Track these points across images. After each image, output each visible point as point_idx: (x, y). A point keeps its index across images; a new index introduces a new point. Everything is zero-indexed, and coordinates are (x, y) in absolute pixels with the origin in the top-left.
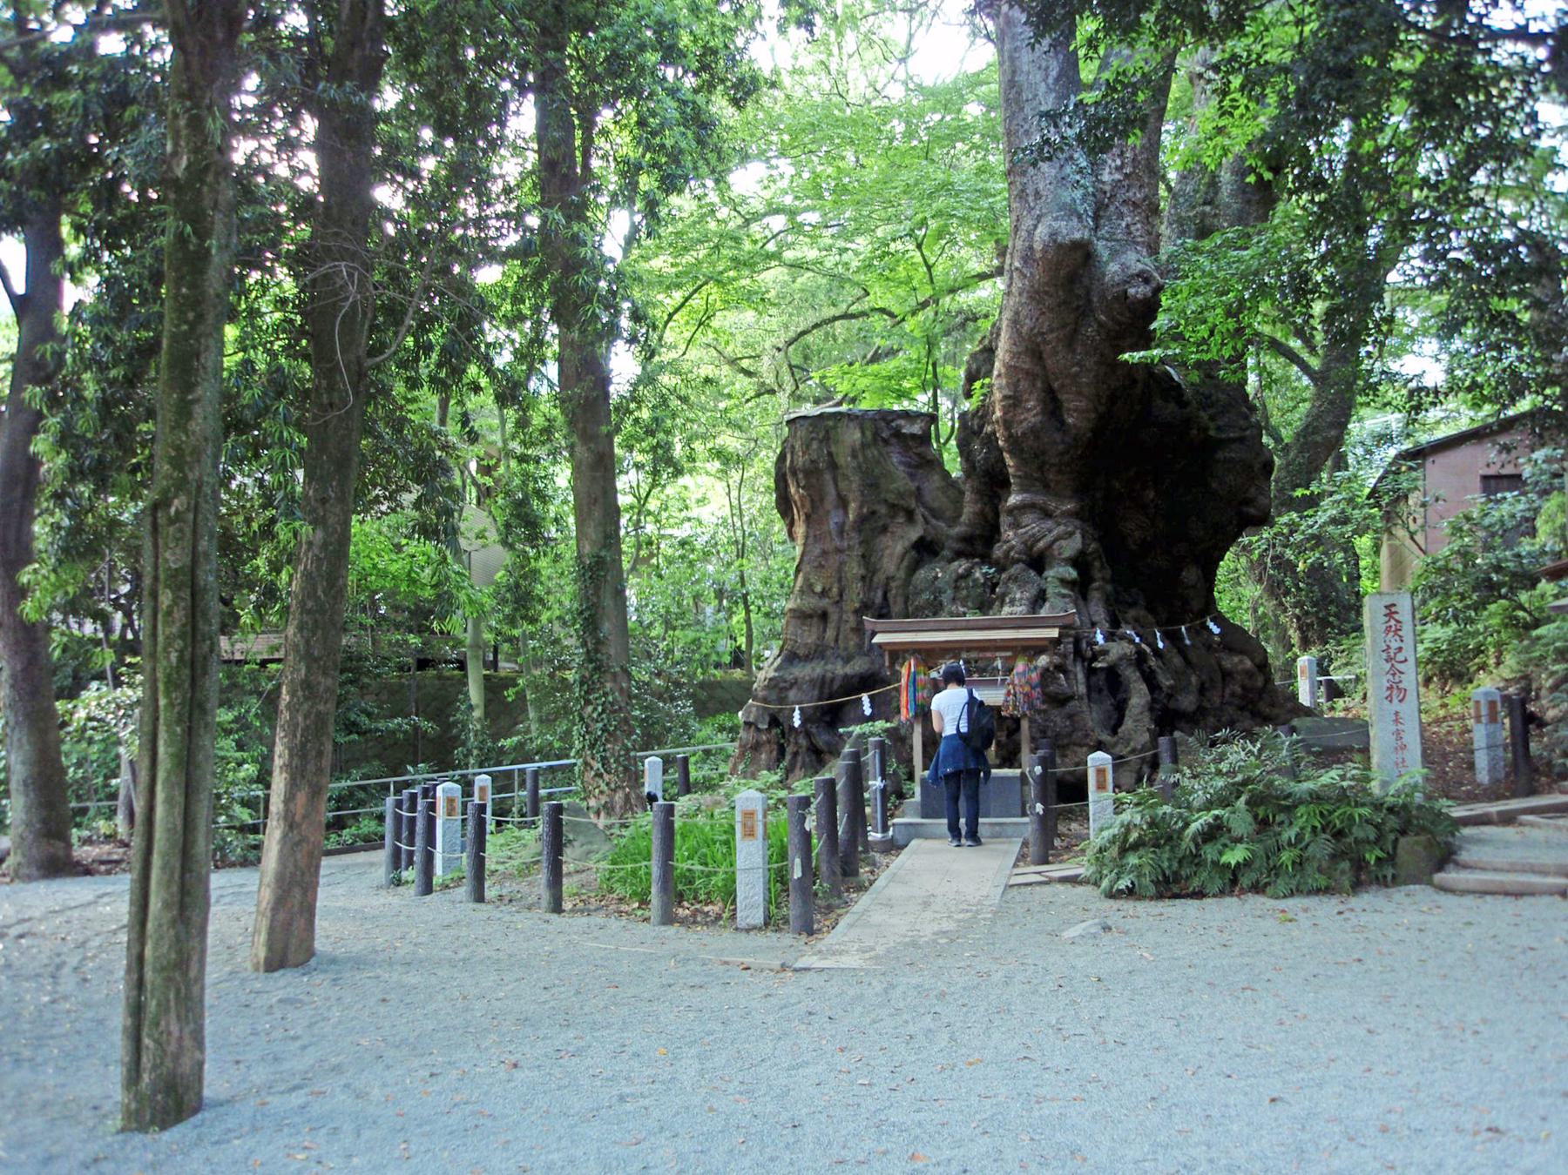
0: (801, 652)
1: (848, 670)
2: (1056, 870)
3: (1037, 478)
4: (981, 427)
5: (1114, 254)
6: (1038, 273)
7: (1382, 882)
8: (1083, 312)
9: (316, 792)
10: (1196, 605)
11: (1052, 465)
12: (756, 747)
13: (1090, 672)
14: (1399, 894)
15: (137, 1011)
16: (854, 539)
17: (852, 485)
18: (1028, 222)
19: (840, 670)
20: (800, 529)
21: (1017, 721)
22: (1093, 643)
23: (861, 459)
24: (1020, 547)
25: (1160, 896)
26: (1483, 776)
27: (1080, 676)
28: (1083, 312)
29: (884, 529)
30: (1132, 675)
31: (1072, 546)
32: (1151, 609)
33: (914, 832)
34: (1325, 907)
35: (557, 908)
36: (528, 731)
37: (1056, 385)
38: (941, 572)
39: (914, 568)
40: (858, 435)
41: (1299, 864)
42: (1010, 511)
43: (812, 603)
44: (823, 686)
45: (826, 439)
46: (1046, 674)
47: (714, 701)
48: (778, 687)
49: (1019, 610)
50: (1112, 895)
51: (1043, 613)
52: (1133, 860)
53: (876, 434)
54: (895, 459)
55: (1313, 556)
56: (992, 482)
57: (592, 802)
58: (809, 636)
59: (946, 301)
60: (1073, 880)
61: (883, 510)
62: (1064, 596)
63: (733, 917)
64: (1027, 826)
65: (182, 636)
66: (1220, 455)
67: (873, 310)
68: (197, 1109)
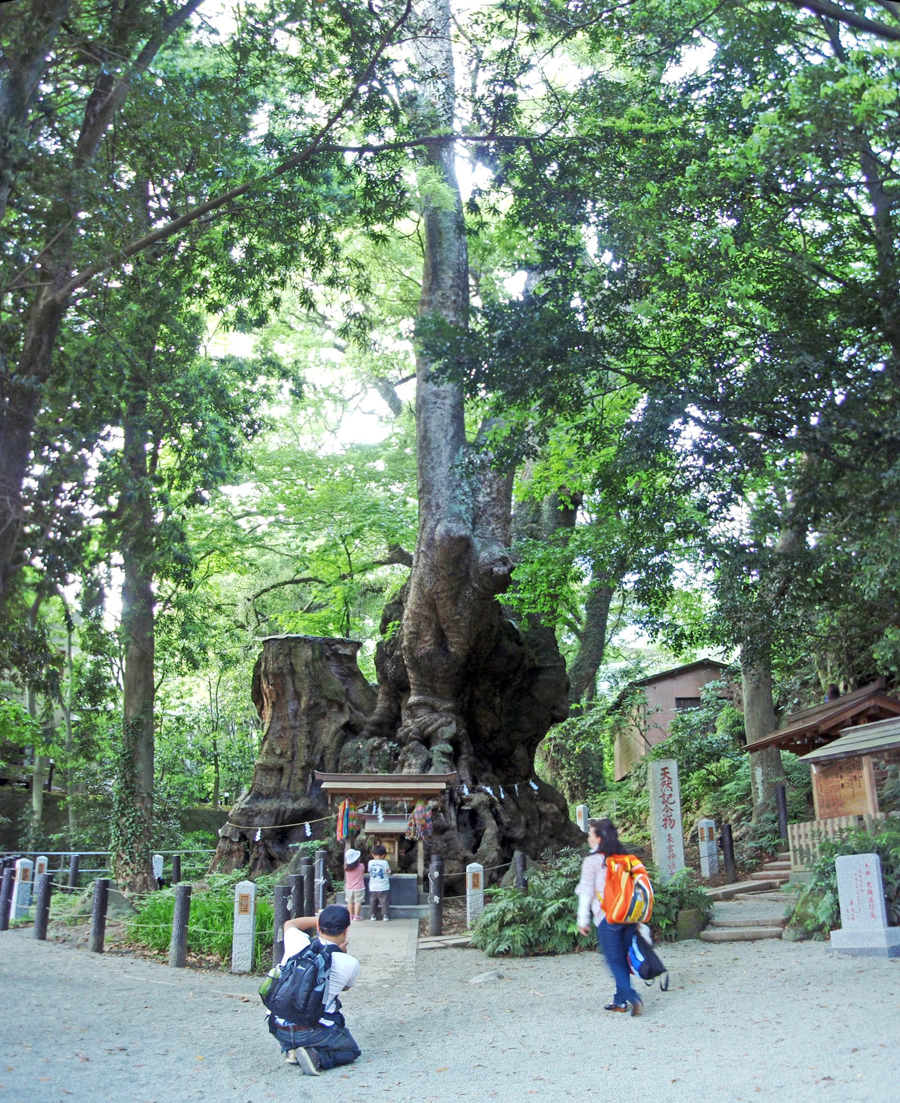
0: (264, 793)
4: (392, 653)
5: (484, 546)
6: (437, 555)
10: (523, 772)
12: (230, 853)
13: (459, 812)
16: (305, 720)
17: (305, 687)
18: (431, 523)
19: (290, 805)
20: (268, 712)
21: (413, 843)
22: (461, 794)
24: (416, 730)
25: (527, 955)
27: (453, 815)
28: (465, 580)
29: (324, 715)
30: (486, 814)
31: (450, 731)
35: (99, 949)
36: (68, 831)
38: (363, 745)
39: (342, 742)
40: (310, 653)
42: (410, 707)
43: (273, 761)
44: (278, 815)
45: (289, 655)
46: (434, 810)
48: (247, 815)
49: (415, 771)
50: (493, 955)
51: (431, 772)
52: (508, 932)
53: (322, 653)
54: (333, 670)
55: (584, 744)
56: (397, 688)
57: (120, 881)
58: (270, 783)
59: (357, 577)
60: (463, 946)
61: (323, 703)
63: (229, 965)
64: (427, 911)
66: (540, 677)
67: (315, 579)
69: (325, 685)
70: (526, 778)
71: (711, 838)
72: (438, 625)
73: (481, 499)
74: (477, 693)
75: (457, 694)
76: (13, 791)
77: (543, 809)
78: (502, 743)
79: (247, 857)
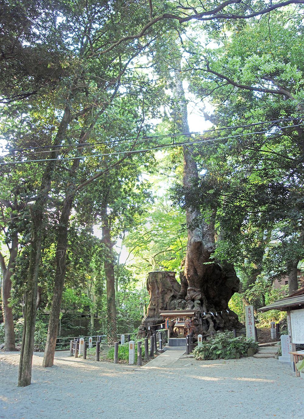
1: (159, 319)
2: (189, 356)
3: (193, 285)
5: (206, 243)
6: (192, 247)
7: (245, 357)
8: (201, 254)
9: (54, 338)
12: (142, 333)
13: (203, 320)
14: (247, 358)
15: (21, 368)
17: (160, 286)
20: (151, 293)
26: (272, 338)
29: (166, 293)
30: (210, 321)
31: (199, 297)
32: (215, 308)
33: (167, 349)
34: (232, 362)
35: (98, 360)
36: (102, 329)
38: (176, 301)
39: (172, 300)
41: (230, 354)
44: (154, 322)
45: (155, 277)
47: (137, 324)
53: (165, 276)
56: (185, 285)
57: (109, 343)
61: (166, 290)
65: (30, 312)
66: (228, 280)
68: (30, 384)
69: (166, 285)
70: (226, 309)
72: (194, 267)
73: (205, 230)
74: (209, 285)
75: (202, 286)
76: (86, 319)
77: (230, 318)
78: (217, 299)
79: (146, 334)
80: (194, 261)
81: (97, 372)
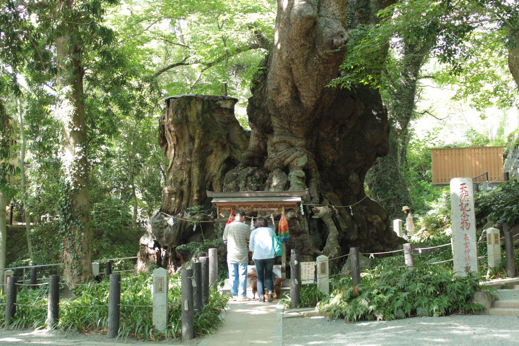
11: (294, 122)
23: (201, 119)
27: (306, 222)
28: (313, 49)
30: (330, 222)
31: (302, 161)
37: (297, 84)
39: (224, 172)
53: (209, 107)
62: (299, 184)
71: (496, 242)
75: (308, 136)
80: (294, 67)
81: (369, 325)
